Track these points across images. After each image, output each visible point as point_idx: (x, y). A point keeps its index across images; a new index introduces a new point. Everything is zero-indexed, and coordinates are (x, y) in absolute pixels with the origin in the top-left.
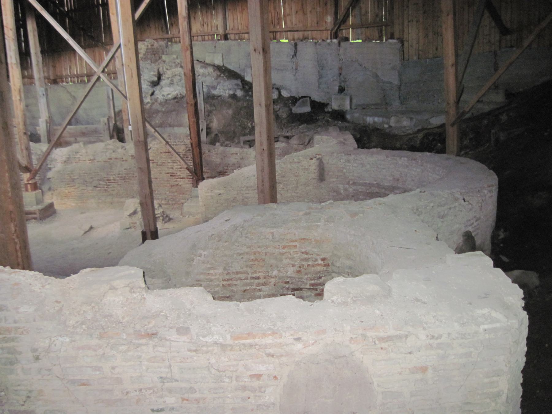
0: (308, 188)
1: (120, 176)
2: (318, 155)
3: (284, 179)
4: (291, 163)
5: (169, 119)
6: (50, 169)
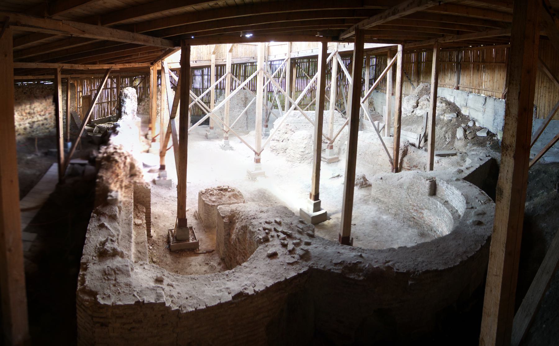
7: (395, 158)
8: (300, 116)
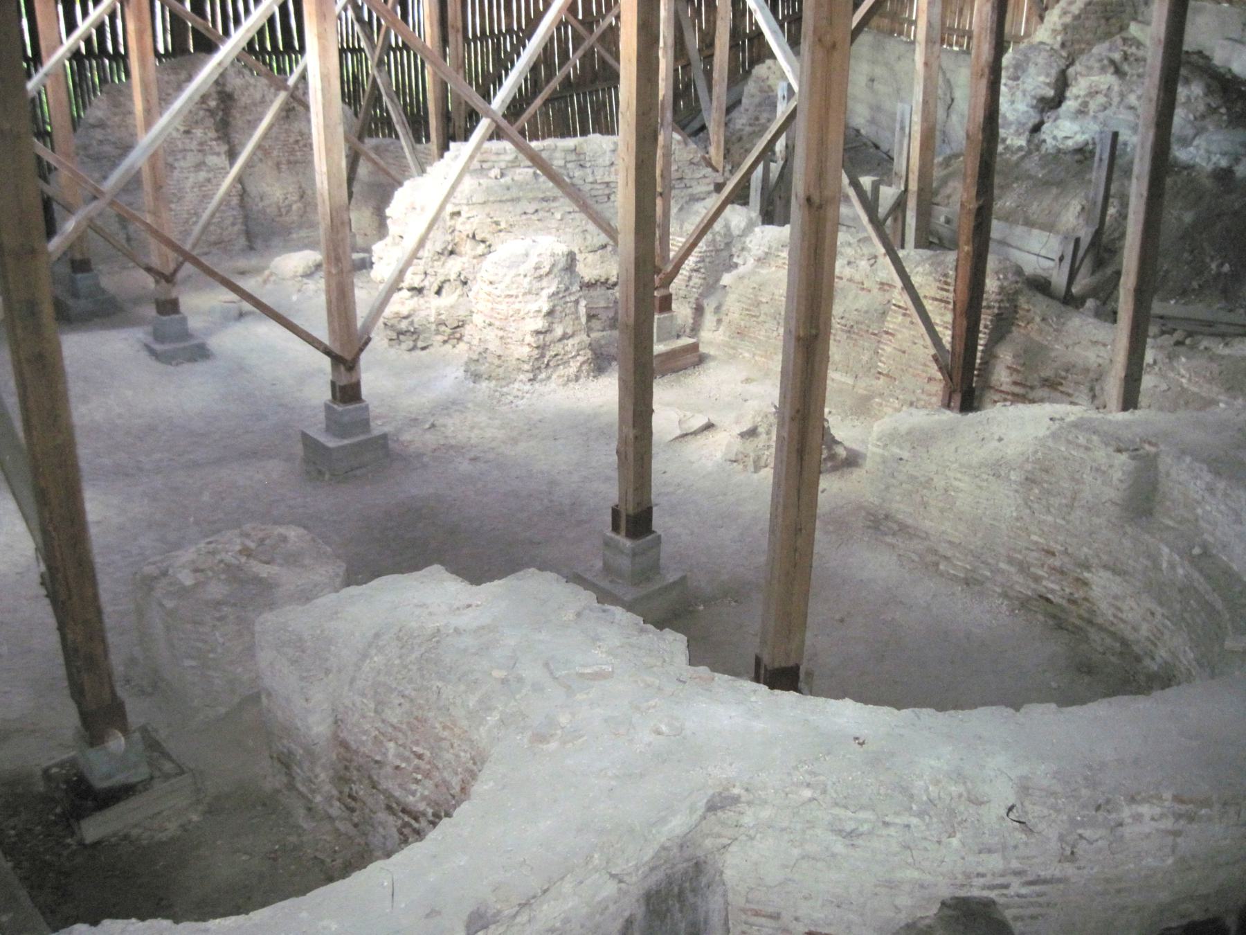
0: (1096, 521)
1: (843, 322)
2: (1150, 443)
3: (1046, 477)
4: (1069, 442)
5: (1035, 204)
6: (736, 266)
7: (960, 348)
8: (514, 164)
